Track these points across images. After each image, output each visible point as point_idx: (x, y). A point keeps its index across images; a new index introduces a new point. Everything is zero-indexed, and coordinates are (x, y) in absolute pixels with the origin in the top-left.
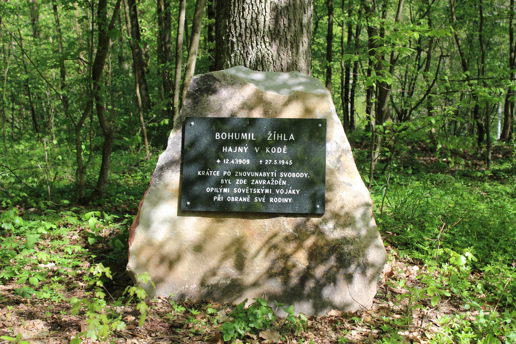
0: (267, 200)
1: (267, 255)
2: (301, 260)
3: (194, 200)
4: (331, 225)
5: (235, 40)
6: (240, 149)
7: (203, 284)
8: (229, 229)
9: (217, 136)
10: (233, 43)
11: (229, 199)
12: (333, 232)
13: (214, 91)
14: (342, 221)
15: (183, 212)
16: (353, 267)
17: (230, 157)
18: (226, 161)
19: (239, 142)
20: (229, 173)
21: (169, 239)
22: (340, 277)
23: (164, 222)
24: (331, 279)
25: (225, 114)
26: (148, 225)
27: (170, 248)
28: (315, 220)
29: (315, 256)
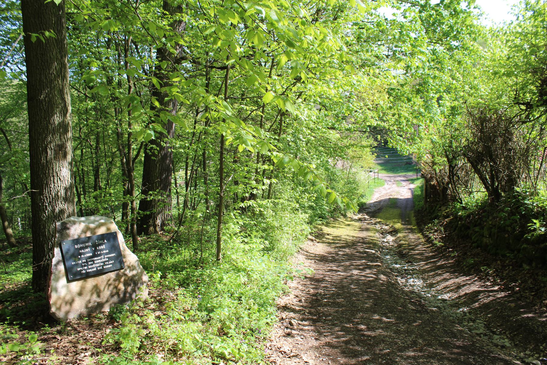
0: (103, 267)
1: (108, 289)
2: (122, 287)
3: (72, 275)
4: (128, 271)
5: (47, 204)
6: (87, 250)
7: (87, 307)
8: (91, 283)
9: (76, 246)
10: (46, 206)
11: (88, 271)
12: (130, 274)
13: (68, 229)
14: (132, 268)
15: (69, 281)
16: (139, 285)
17: (84, 254)
18: (83, 256)
19: (87, 247)
20: (85, 261)
21: (67, 294)
22: (136, 289)
23: (63, 287)
24: (134, 291)
25: (76, 237)
26: (56, 290)
27: (68, 298)
28: (122, 271)
29: (126, 284)
